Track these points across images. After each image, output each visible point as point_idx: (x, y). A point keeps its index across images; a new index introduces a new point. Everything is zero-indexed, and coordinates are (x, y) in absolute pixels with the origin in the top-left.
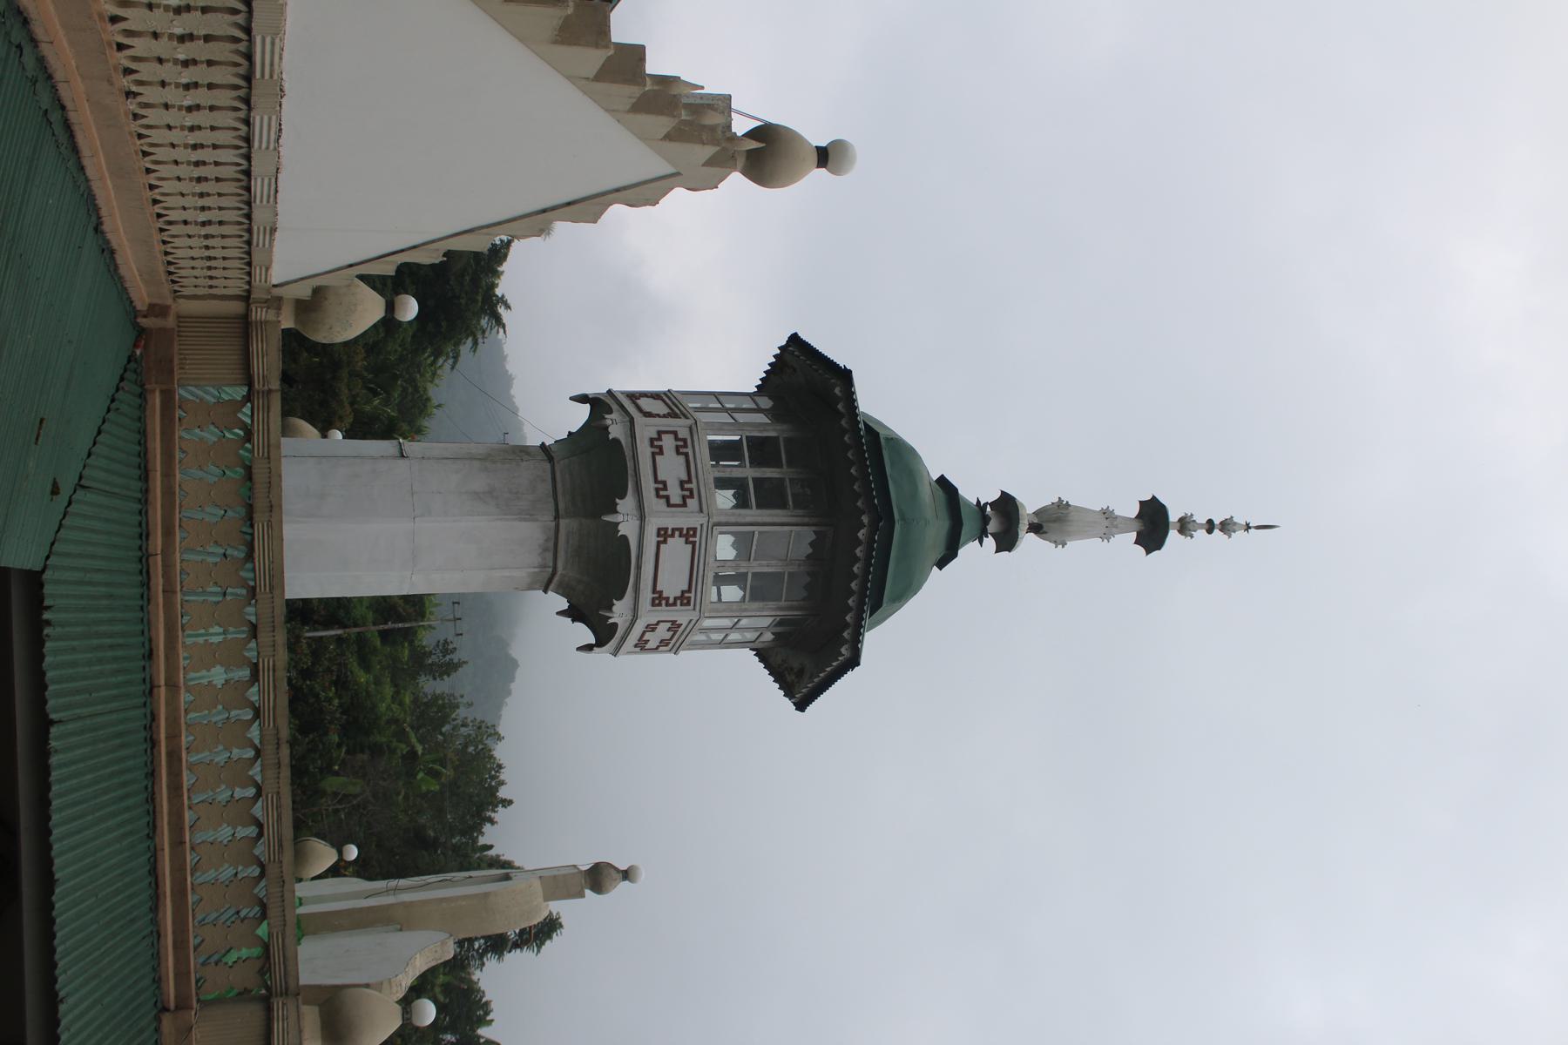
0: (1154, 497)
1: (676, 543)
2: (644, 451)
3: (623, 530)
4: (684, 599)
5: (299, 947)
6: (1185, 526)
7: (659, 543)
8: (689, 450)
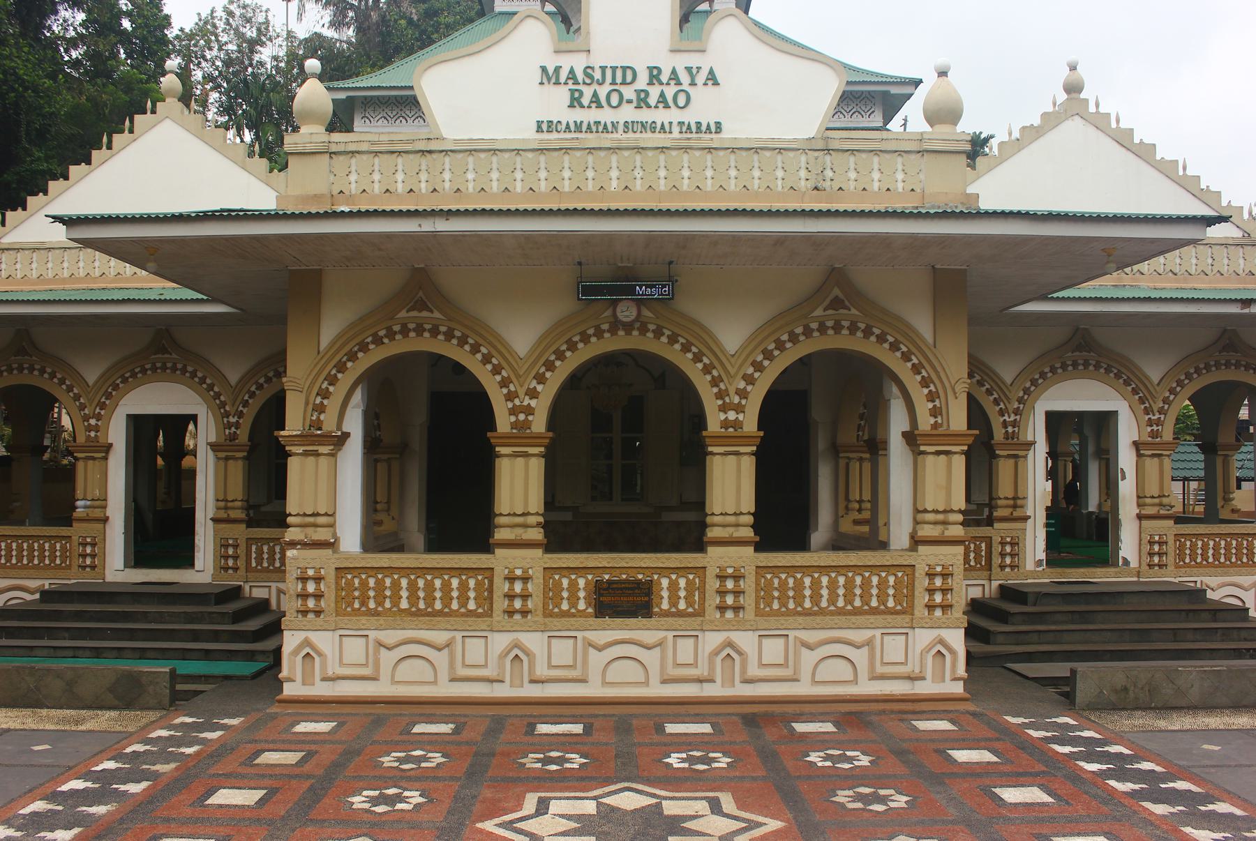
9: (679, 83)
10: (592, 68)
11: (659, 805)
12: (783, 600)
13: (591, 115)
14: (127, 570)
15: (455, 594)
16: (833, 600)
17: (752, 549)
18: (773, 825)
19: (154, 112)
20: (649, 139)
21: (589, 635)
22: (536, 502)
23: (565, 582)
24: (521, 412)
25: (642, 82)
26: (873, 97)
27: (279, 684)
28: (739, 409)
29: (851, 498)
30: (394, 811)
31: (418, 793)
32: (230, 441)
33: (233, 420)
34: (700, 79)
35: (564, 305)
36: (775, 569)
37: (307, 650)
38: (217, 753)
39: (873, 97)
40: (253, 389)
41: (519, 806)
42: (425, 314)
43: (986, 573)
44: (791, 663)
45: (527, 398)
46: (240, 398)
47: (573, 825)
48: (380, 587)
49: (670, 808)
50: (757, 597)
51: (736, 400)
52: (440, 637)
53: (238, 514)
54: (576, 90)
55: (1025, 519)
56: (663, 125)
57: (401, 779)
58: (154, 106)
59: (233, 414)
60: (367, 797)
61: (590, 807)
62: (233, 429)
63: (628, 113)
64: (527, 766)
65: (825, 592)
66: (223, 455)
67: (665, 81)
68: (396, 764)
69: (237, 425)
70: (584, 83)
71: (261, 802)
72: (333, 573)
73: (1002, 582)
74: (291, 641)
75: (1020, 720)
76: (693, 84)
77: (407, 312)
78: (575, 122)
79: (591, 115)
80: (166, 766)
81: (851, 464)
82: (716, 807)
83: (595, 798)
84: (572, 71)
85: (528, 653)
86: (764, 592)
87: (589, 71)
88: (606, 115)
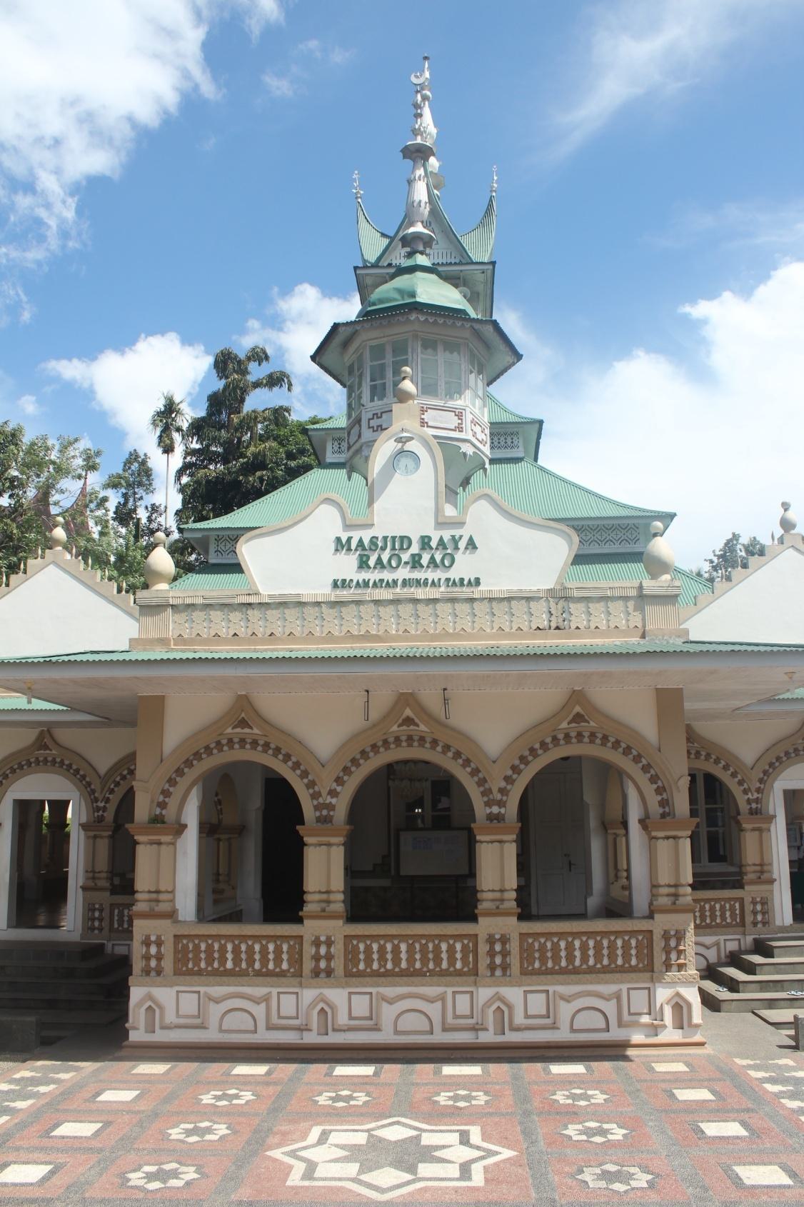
0: (401, 151)
4: (459, 416)
7: (428, 426)
9: (445, 548)
10: (377, 538)
11: (418, 1138)
12: (543, 960)
13: (373, 576)
14: (10, 930)
15: (271, 956)
16: (585, 958)
17: (515, 919)
18: (507, 1153)
19: (43, 557)
20: (420, 593)
21: (381, 990)
22: (338, 881)
23: (362, 946)
24: (324, 809)
25: (415, 549)
26: (637, 528)
27: (126, 1034)
28: (501, 804)
29: (619, 867)
30: (203, 1141)
31: (225, 1126)
32: (98, 822)
33: (102, 805)
34: (462, 544)
36: (536, 935)
37: (149, 1003)
38: (67, 1093)
39: (637, 528)
40: (118, 779)
41: (304, 1136)
42: (247, 730)
43: (741, 929)
44: (551, 1015)
45: (329, 797)
46: (107, 786)
47: (437, 1154)
48: (210, 950)
49: (427, 1140)
50: (521, 958)
51: (499, 797)
52: (259, 991)
53: (103, 883)
54: (365, 555)
55: (772, 881)
56: (433, 580)
57: (214, 1113)
58: (43, 552)
59: (101, 800)
60: (183, 1129)
61: (361, 1138)
62: (101, 813)
63: (403, 573)
64: (320, 1103)
65: (577, 953)
66: (92, 834)
67: (434, 547)
68: (213, 1101)
69: (104, 809)
70: (371, 549)
71: (97, 1133)
72: (172, 939)
73: (757, 936)
74: (137, 993)
75: (745, 1062)
77: (233, 729)
78: (364, 580)
79: (373, 576)
80: (24, 1103)
81: (618, 839)
82: (465, 1139)
83: (368, 1131)
84: (361, 541)
85: (332, 1007)
86: (527, 955)
87: (374, 540)
88: (387, 576)
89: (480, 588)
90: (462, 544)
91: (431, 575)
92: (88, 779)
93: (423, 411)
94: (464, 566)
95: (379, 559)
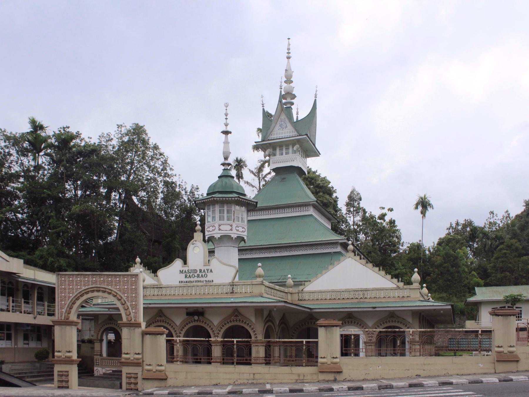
1: (221, 227)
2: (238, 232)
3: (219, 236)
5: (22, 261)
6: (226, 125)
8: (209, 226)
9: (205, 272)
20: (189, 284)
25: (198, 273)
34: (209, 271)
35: (185, 317)
63: (196, 279)
76: (208, 272)
88: (192, 279)
89: (213, 283)
90: (209, 271)
91: (202, 279)
92: (254, 329)
93: (220, 226)
94: (210, 277)
95: (202, 275)
